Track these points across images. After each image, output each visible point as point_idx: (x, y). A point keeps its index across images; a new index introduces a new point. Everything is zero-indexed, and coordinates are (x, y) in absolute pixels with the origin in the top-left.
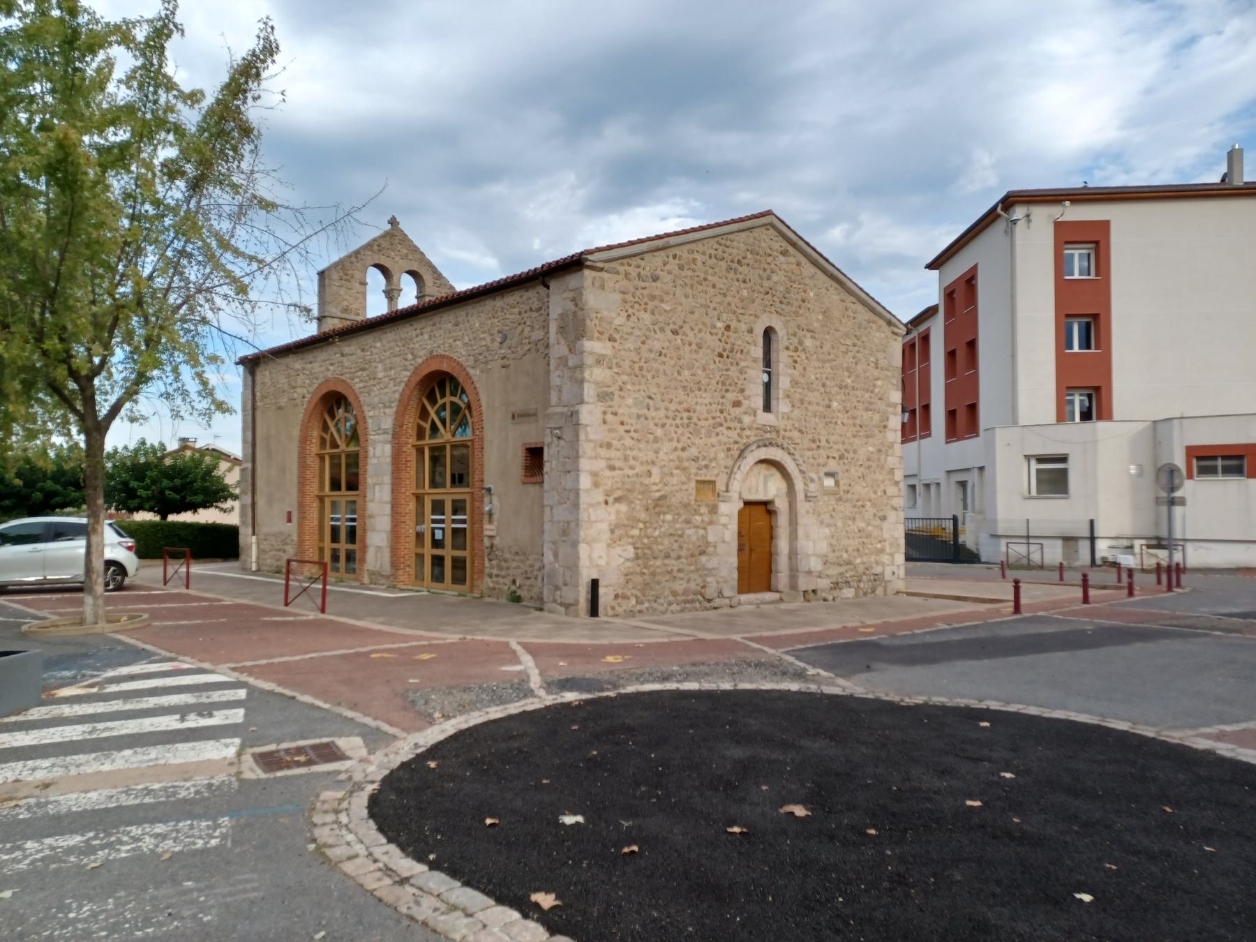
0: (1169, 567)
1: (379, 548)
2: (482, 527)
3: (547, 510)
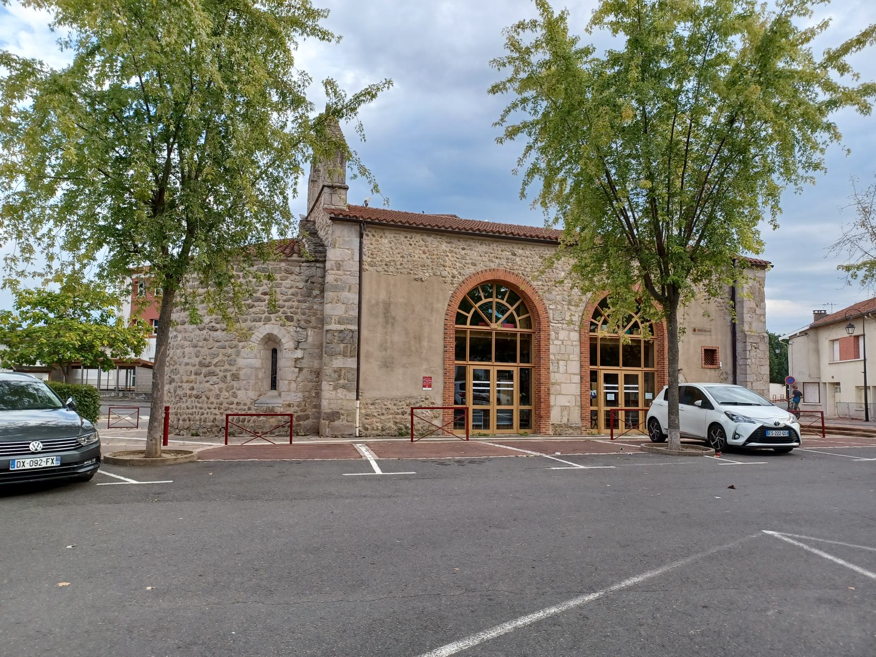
1: (564, 408)
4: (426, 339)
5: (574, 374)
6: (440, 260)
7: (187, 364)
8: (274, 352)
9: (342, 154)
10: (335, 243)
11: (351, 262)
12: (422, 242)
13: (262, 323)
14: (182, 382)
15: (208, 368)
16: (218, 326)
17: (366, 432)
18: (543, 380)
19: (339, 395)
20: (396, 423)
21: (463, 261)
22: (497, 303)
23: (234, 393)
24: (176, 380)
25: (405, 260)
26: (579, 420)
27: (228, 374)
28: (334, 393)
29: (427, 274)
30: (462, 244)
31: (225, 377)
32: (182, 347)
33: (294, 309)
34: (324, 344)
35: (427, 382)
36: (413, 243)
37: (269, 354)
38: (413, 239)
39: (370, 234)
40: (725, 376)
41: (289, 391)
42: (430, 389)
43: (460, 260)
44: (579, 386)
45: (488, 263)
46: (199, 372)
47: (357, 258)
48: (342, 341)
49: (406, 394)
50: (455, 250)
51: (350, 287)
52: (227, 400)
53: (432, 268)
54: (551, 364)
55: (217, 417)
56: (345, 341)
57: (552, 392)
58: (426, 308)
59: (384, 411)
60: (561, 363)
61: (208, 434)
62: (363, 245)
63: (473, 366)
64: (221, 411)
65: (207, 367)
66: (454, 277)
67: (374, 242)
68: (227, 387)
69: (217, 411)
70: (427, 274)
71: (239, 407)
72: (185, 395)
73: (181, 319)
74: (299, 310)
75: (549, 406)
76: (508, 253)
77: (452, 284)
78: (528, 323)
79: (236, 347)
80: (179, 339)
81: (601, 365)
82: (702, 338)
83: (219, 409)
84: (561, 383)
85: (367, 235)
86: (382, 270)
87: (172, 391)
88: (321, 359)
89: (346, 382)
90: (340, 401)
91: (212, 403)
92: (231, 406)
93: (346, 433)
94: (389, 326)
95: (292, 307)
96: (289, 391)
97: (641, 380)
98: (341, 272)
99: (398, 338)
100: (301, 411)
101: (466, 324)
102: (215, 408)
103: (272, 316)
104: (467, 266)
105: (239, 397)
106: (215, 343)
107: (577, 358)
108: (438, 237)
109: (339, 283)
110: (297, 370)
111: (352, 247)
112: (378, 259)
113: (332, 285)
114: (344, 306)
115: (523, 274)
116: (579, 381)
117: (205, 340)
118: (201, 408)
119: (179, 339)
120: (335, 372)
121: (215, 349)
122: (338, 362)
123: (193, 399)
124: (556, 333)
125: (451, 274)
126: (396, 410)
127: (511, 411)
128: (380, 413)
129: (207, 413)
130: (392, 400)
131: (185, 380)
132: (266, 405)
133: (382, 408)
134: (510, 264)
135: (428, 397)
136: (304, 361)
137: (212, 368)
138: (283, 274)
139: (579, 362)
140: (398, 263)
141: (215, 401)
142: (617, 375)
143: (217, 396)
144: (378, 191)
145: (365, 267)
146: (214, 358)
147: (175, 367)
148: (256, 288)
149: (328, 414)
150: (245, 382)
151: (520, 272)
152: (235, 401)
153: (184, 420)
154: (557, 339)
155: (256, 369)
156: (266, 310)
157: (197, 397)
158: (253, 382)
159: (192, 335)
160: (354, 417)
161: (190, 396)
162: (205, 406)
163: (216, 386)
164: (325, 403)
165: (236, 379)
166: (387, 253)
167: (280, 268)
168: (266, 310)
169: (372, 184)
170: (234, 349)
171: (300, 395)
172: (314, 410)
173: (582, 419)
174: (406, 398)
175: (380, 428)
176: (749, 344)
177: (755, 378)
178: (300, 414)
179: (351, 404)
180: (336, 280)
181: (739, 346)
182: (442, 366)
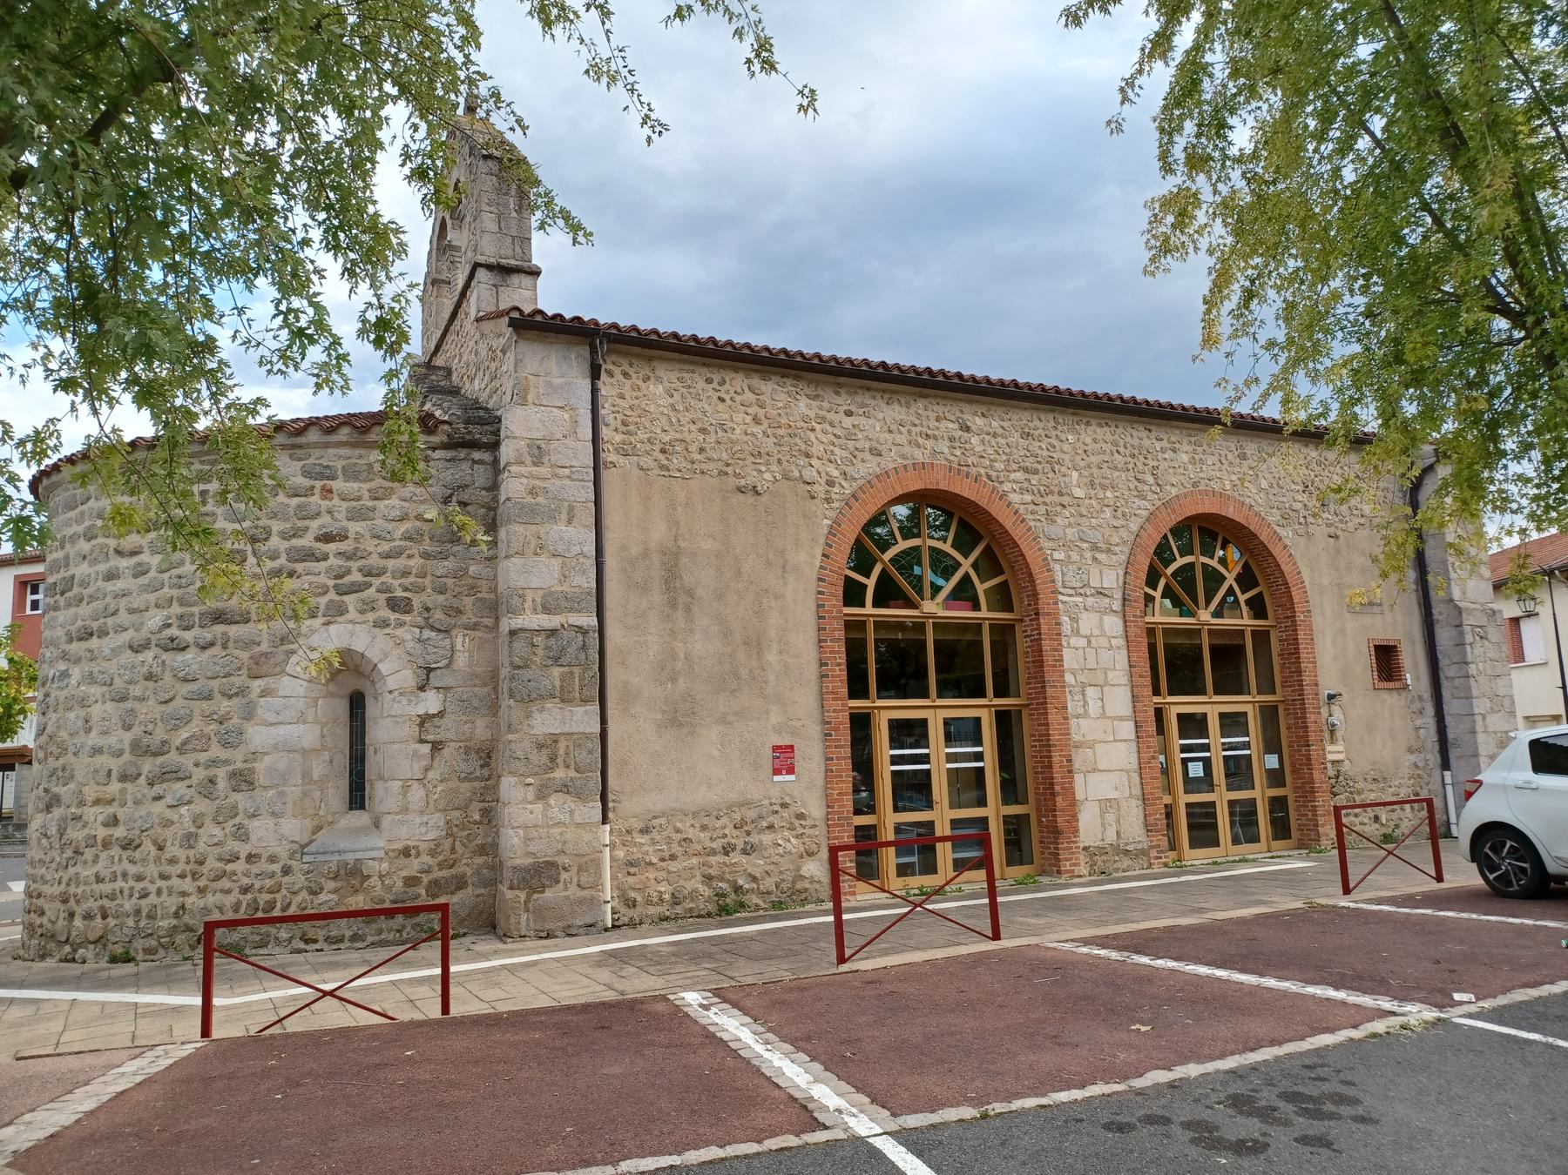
0: (1050, 746)
1: (1107, 804)
2: (1323, 750)
3: (1478, 719)
4: (775, 646)
5: (1121, 719)
6: (798, 441)
7: (97, 751)
8: (357, 704)
9: (522, 195)
10: (526, 391)
11: (570, 442)
12: (749, 396)
13: (320, 620)
14: (81, 803)
15: (160, 760)
16: (188, 636)
17: (631, 912)
18: (1055, 737)
19: (556, 813)
20: (708, 879)
21: (851, 444)
22: (932, 549)
23: (240, 827)
24: (65, 799)
25: (711, 439)
26: (1142, 831)
27: (221, 773)
28: (539, 806)
29: (767, 476)
30: (844, 401)
31: (212, 781)
32: (83, 702)
33: (412, 579)
34: (505, 672)
35: (784, 759)
36: (727, 397)
37: (342, 707)
38: (727, 386)
39: (617, 371)
40: (1418, 705)
41: (405, 810)
42: (792, 777)
43: (842, 441)
44: (1134, 745)
45: (907, 450)
46: (133, 770)
47: (587, 433)
48: (556, 661)
49: (733, 796)
50: (830, 416)
51: (571, 509)
52: (218, 850)
53: (779, 461)
54: (1069, 697)
55: (189, 901)
56: (564, 660)
57: (1077, 765)
58: (768, 563)
59: (676, 849)
60: (1090, 691)
61: (162, 953)
62: (601, 401)
63: (887, 710)
64: (202, 883)
65: (155, 754)
66: (830, 483)
67: (627, 391)
68: (218, 811)
69: (188, 885)
70: (767, 476)
71: (255, 869)
72: (91, 841)
73: (79, 623)
74: (427, 581)
75: (1073, 803)
76: (951, 425)
77: (828, 500)
78: (1002, 597)
79: (242, 692)
80: (73, 681)
81: (1216, 693)
82: (1367, 620)
83: (195, 876)
84: (1096, 741)
85: (610, 374)
86: (652, 464)
87: (53, 831)
88: (495, 715)
89: (572, 773)
90: (555, 831)
91: (173, 861)
92: (230, 867)
93: (578, 922)
94: (680, 613)
95: (406, 573)
96: (405, 810)
97: (1253, 724)
98: (544, 471)
99: (703, 645)
100: (441, 866)
101: (863, 605)
102: (182, 876)
103: (346, 598)
104: (860, 455)
105: (253, 838)
106: (178, 685)
107: (1124, 680)
108: (789, 381)
109: (540, 500)
110: (426, 748)
111: (573, 401)
112: (642, 435)
113: (522, 506)
114: (556, 562)
115: (989, 477)
116: (1133, 736)
117: (149, 677)
118: (139, 878)
119: (73, 681)
120: (540, 746)
121: (179, 701)
122: (548, 720)
123: (115, 851)
124: (1072, 619)
125: (825, 477)
126: (709, 844)
127: (985, 820)
128: (666, 854)
129: (159, 892)
130: (695, 814)
131: (90, 799)
132: (336, 857)
133: (669, 841)
134: (958, 452)
135: (787, 800)
136: (447, 721)
137: (173, 756)
138: (379, 482)
139: (1128, 688)
140: (694, 448)
141: (181, 854)
142: (923, 723)
143: (189, 840)
144: (770, 66)
145: (609, 456)
146: (176, 728)
147: (62, 761)
148: (300, 524)
149: (526, 870)
150: (270, 793)
151: (982, 471)
152: (244, 850)
153: (88, 916)
154: (1077, 633)
155: (305, 753)
156: (331, 583)
157: (128, 845)
158: (297, 791)
159: (112, 667)
160: (598, 874)
161: (106, 845)
162: (152, 870)
163: (183, 810)
164: (516, 840)
165: (244, 786)
166: (664, 420)
167: (370, 466)
168: (331, 583)
169: (750, 39)
170: (235, 700)
171: (438, 819)
172: (479, 860)
173: (1149, 828)
174: (731, 807)
175: (667, 897)
176: (1467, 629)
177: (1489, 704)
178: (437, 874)
179: (587, 837)
180: (532, 492)
181: (1443, 636)
182: (817, 715)
